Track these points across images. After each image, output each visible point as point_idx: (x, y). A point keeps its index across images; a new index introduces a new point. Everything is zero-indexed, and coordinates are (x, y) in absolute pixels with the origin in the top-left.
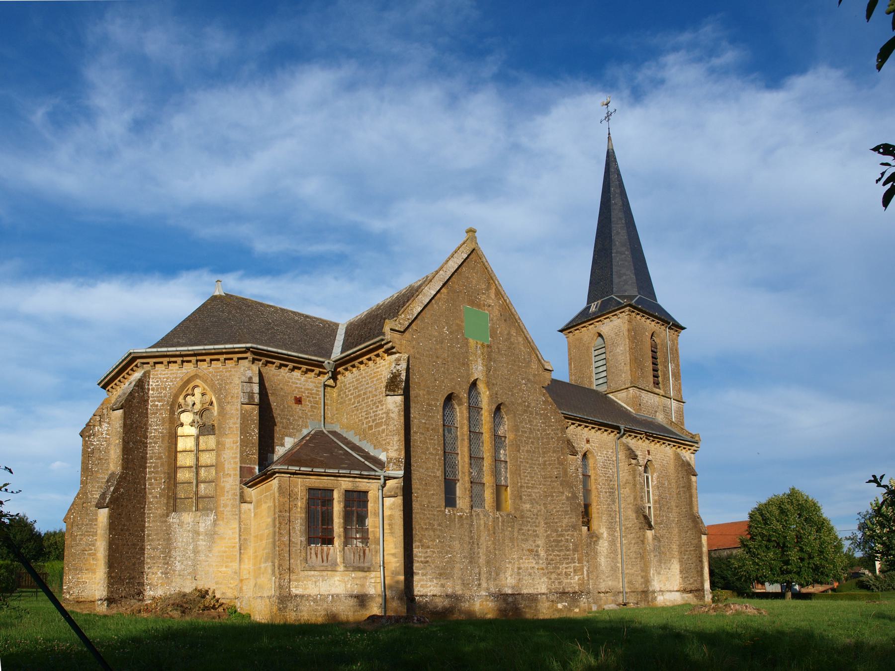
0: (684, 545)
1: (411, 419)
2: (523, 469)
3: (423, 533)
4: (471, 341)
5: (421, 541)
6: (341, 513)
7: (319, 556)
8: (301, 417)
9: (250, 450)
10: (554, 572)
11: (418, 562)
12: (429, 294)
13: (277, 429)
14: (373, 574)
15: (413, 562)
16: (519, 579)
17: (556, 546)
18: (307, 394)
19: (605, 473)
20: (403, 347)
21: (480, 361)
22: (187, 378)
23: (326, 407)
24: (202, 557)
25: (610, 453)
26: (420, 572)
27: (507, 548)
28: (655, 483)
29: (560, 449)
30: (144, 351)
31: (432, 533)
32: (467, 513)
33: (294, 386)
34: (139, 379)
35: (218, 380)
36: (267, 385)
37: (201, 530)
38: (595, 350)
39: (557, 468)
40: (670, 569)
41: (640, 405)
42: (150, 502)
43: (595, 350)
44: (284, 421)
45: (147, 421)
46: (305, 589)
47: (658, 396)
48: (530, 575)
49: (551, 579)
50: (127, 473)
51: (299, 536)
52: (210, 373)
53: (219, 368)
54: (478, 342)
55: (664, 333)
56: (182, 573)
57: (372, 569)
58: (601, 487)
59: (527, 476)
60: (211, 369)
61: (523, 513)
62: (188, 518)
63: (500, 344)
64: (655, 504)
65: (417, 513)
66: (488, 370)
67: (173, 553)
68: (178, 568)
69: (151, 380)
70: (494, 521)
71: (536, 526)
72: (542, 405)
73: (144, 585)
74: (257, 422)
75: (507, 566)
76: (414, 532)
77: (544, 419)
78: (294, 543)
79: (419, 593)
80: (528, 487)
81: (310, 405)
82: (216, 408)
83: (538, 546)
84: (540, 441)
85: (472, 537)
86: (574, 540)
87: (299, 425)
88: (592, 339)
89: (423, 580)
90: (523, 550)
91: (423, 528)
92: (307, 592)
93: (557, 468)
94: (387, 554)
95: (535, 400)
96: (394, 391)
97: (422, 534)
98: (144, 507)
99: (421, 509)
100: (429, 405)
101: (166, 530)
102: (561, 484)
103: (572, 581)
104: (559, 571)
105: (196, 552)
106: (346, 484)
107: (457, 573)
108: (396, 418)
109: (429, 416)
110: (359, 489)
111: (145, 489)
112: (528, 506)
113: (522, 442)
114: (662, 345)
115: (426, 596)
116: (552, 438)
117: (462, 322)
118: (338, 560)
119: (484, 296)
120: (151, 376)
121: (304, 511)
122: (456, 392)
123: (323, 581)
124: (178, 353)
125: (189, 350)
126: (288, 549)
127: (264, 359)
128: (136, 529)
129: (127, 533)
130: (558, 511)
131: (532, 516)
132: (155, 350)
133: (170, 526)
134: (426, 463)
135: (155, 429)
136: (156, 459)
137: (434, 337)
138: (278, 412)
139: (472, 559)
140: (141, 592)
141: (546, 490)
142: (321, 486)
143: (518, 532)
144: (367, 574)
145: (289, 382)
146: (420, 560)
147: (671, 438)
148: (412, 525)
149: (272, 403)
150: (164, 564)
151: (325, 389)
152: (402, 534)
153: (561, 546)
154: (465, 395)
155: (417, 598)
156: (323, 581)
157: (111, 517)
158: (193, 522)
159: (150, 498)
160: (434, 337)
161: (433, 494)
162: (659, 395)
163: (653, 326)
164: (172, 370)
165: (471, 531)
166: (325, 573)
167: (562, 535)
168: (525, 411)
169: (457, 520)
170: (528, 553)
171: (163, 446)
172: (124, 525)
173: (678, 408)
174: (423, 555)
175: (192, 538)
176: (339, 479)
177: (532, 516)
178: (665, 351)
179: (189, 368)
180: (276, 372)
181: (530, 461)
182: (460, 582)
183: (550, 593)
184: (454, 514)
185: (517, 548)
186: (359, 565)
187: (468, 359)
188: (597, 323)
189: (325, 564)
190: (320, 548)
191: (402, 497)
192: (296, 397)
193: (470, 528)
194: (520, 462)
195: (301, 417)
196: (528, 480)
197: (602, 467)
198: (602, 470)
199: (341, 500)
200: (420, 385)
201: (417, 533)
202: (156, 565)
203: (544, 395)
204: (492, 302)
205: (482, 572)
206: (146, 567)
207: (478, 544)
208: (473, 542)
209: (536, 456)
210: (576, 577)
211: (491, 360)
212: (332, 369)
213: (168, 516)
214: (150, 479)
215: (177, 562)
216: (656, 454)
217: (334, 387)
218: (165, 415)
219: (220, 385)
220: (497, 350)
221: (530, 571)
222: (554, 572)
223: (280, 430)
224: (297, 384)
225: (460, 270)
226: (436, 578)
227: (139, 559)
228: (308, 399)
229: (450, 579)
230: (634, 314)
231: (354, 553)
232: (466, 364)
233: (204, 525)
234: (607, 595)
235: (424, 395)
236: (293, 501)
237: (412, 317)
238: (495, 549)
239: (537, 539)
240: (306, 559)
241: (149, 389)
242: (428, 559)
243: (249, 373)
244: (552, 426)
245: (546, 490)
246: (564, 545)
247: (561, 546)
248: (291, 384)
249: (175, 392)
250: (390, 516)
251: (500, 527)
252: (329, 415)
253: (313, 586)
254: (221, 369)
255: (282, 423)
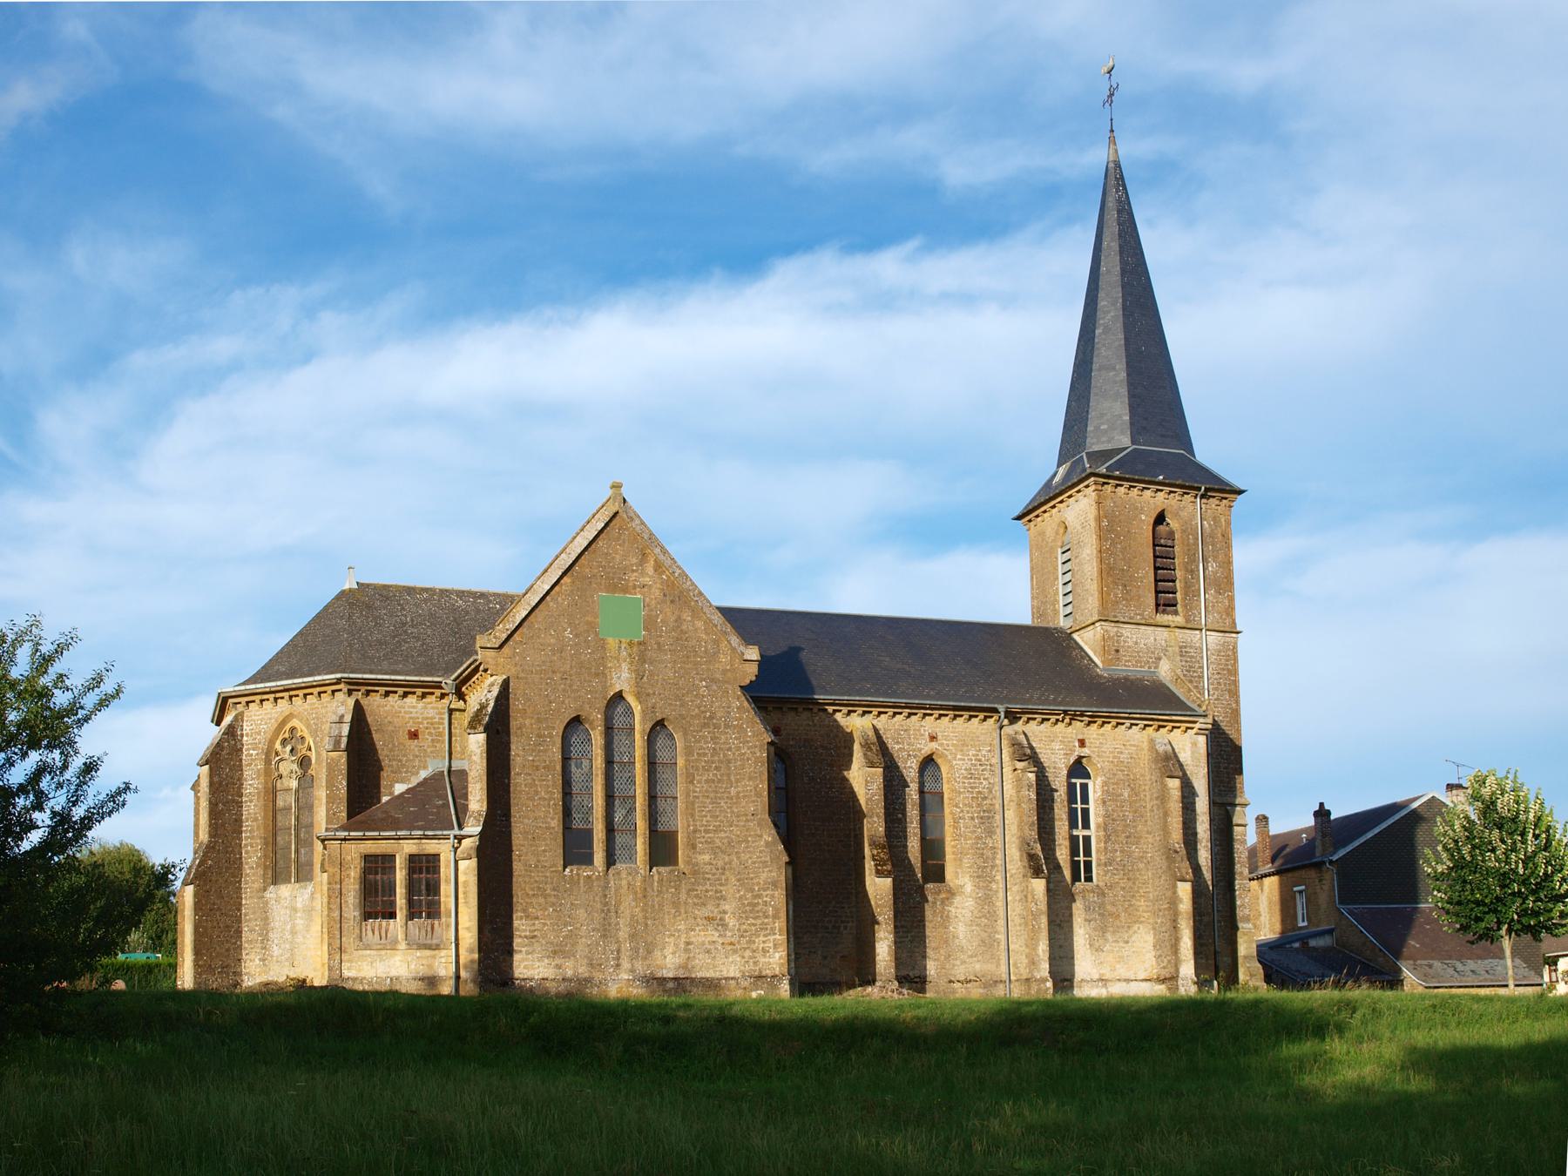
0: (1157, 901)
1: (512, 757)
2: (698, 807)
3: (529, 901)
4: (610, 640)
5: (524, 911)
6: (404, 882)
7: (377, 932)
8: (417, 756)
9: (337, 807)
10: (748, 948)
11: (520, 937)
12: (541, 590)
13: (384, 774)
14: (443, 953)
15: (513, 937)
16: (689, 958)
17: (751, 911)
18: (426, 725)
19: (971, 788)
20: (500, 667)
21: (625, 666)
22: (281, 719)
23: (453, 739)
24: (300, 939)
25: (984, 753)
26: (523, 949)
27: (666, 916)
28: (1099, 794)
29: (757, 775)
30: (232, 690)
31: (543, 900)
32: (599, 872)
33: (407, 716)
34: (229, 725)
35: (313, 719)
36: (369, 720)
37: (299, 905)
38: (1063, 553)
39: (754, 801)
40: (1127, 942)
41: (1117, 651)
42: (247, 875)
43: (1063, 553)
44: (394, 763)
45: (242, 774)
46: (359, 971)
47: (1168, 629)
48: (708, 952)
49: (743, 957)
50: (216, 842)
51: (352, 911)
52: (305, 710)
53: (314, 704)
54: (623, 640)
55: (1190, 507)
56: (279, 959)
57: (442, 947)
58: (962, 811)
59: (706, 816)
60: (306, 706)
61: (696, 868)
62: (285, 890)
63: (661, 636)
64: (1097, 831)
65: (520, 876)
66: (640, 676)
67: (271, 935)
68: (275, 954)
69: (245, 724)
70: (645, 881)
71: (721, 885)
72: (735, 713)
73: (241, 975)
74: (345, 772)
75: (667, 940)
76: (515, 900)
77: (738, 732)
78: (346, 918)
79: (521, 976)
80: (707, 831)
81: (430, 738)
82: (314, 754)
83: (725, 912)
84: (731, 765)
85: (607, 902)
86: (775, 902)
87: (414, 767)
88: (1057, 533)
89: (527, 959)
90: (695, 918)
91: (528, 895)
92: (362, 974)
93: (754, 801)
94: (463, 928)
95: (723, 707)
96: (475, 728)
97: (527, 903)
98: (240, 880)
99: (526, 870)
100: (539, 736)
101: (264, 907)
102: (759, 824)
103: (771, 960)
104: (754, 947)
105: (293, 933)
106: (409, 847)
107: (581, 949)
108: (479, 761)
109: (540, 751)
110: (426, 852)
111: (241, 858)
112: (707, 857)
113: (697, 770)
114: (1184, 531)
115: (531, 980)
116: (748, 759)
117: (595, 618)
118: (399, 937)
119: (635, 574)
120: (245, 718)
121: (358, 881)
122: (583, 714)
123: (380, 962)
124: (268, 690)
125: (277, 686)
126: (338, 926)
127: (363, 689)
128: (229, 907)
129: (218, 913)
130: (754, 863)
131: (714, 871)
132: (243, 688)
133: (267, 903)
134: (534, 811)
135: (250, 785)
136: (252, 822)
137: (549, 645)
138: (385, 752)
139: (606, 931)
140: (238, 984)
141: (739, 832)
142: (378, 851)
143: (688, 894)
144: (437, 952)
145: (400, 712)
146: (523, 934)
147: (1130, 713)
148: (511, 890)
149: (377, 743)
150: (263, 948)
151: (450, 715)
152: (476, 903)
153: (758, 912)
154: (599, 716)
155: (517, 982)
156: (380, 962)
157: (196, 895)
158: (291, 896)
159: (247, 870)
160: (549, 645)
161: (544, 851)
162: (1169, 627)
163: (1162, 498)
164: (266, 709)
165: (605, 896)
166: (383, 952)
167: (759, 896)
168: (705, 725)
169: (582, 881)
170: (705, 922)
171: (259, 804)
172: (214, 904)
173: (1223, 645)
174: (528, 928)
175: (290, 916)
176: (401, 841)
177: (714, 871)
178: (1191, 541)
179: (283, 704)
180: (383, 701)
181: (712, 795)
182: (585, 961)
183: (743, 976)
184: (578, 874)
185: (684, 916)
186: (425, 942)
187: (605, 667)
188: (1061, 505)
189: (383, 941)
190: (377, 924)
191: (476, 859)
192: (409, 731)
193: (604, 891)
194: (694, 797)
195: (417, 756)
196: (707, 822)
197: (965, 778)
198: (964, 783)
199: (403, 866)
200: (526, 713)
201: (520, 900)
202: (253, 950)
203: (738, 699)
204: (648, 579)
205: (623, 949)
206: (244, 953)
207: (617, 912)
208: (608, 910)
209: (724, 786)
210: (777, 954)
211: (645, 662)
212: (452, 689)
213: (265, 890)
214: (246, 845)
215: (275, 946)
216: (1101, 743)
217: (464, 711)
218: (261, 766)
219: (316, 725)
220: (656, 646)
221: (709, 947)
222: (748, 948)
223: (387, 776)
224: (411, 713)
225: (593, 546)
226: (548, 957)
227: (235, 943)
228: (427, 731)
229: (569, 958)
230: (1109, 488)
231: (419, 928)
232: (602, 675)
233: (301, 899)
234: (969, 985)
235: (532, 725)
236: (345, 871)
237: (512, 627)
238: (646, 918)
239: (722, 902)
240: (361, 937)
241: (242, 735)
242: (536, 933)
243: (341, 710)
244: (748, 742)
245: (739, 832)
246: (762, 909)
247: (758, 912)
248: (403, 714)
249: (269, 737)
250: (465, 882)
251: (655, 889)
252: (459, 748)
253: (369, 967)
254: (316, 706)
255: (392, 766)
